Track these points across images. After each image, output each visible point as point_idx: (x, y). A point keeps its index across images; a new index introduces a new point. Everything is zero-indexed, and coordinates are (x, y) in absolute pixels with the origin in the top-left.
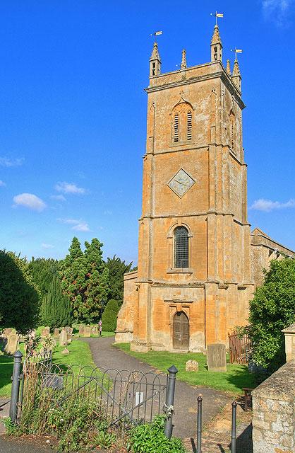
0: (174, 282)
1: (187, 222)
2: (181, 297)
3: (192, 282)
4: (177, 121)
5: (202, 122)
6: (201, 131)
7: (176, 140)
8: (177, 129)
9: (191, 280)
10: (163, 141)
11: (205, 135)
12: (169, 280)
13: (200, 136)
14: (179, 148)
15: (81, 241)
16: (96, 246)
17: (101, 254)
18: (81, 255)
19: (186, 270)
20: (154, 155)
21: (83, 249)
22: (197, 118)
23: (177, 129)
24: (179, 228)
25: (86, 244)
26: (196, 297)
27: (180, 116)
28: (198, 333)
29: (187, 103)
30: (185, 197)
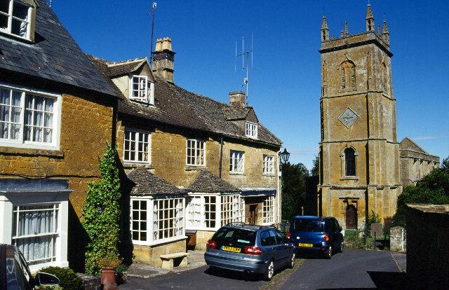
0: (346, 186)
1: (355, 145)
5: (362, 75)
6: (362, 81)
13: (361, 84)
22: (359, 72)
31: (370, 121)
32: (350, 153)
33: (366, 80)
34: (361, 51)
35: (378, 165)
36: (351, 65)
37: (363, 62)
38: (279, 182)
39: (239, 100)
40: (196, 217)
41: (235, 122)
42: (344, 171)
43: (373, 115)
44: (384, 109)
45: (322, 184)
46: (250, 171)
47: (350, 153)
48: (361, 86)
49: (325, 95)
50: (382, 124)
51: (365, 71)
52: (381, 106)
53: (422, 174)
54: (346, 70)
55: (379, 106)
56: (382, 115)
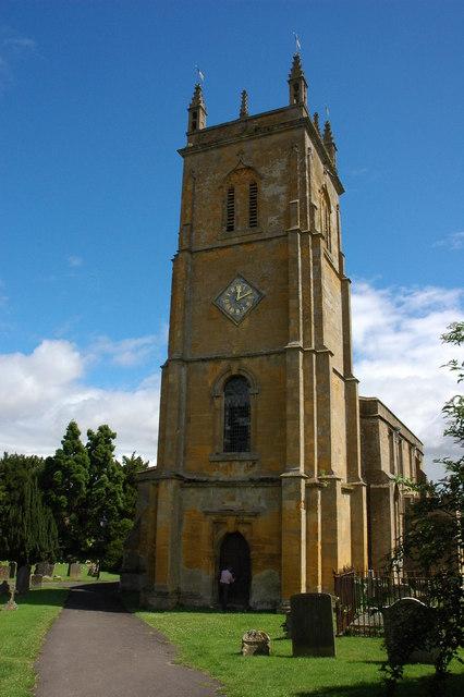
2: (235, 505)
3: (256, 477)
4: (231, 199)
5: (276, 198)
7: (230, 229)
8: (241, 244)
9: (254, 473)
11: (280, 218)
12: (214, 474)
13: (272, 219)
14: (236, 240)
15: (83, 428)
16: (104, 437)
17: (112, 450)
18: (78, 449)
19: (244, 455)
20: (191, 253)
21: (84, 440)
22: (267, 191)
23: (241, 244)
24: (234, 378)
25: (90, 433)
26: (263, 504)
27: (237, 190)
28: (264, 573)
29: (249, 168)
30: (245, 323)
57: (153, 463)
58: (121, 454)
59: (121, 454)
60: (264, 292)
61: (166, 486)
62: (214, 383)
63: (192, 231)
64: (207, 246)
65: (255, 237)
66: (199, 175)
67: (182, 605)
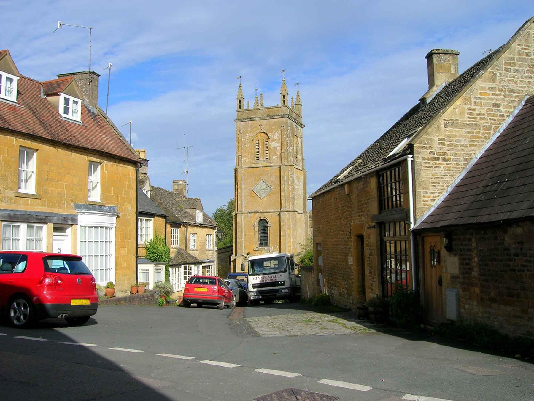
1: (267, 217)
5: (275, 148)
6: (276, 154)
10: (249, 159)
13: (274, 157)
14: (260, 165)
22: (274, 144)
31: (283, 194)
32: (263, 223)
33: (279, 154)
34: (275, 124)
35: (289, 236)
36: (264, 136)
37: (277, 136)
38: (215, 254)
39: (182, 187)
40: (274, 276)
41: (186, 210)
42: (258, 242)
43: (284, 187)
44: (296, 181)
45: (236, 255)
46: (200, 247)
47: (263, 223)
48: (275, 159)
49: (240, 166)
50: (294, 197)
51: (279, 144)
52: (293, 179)
53: (330, 195)
54: (260, 141)
55: (291, 179)
56: (293, 188)
57: (48, 260)
58: (88, 198)
59: (88, 198)
60: (272, 188)
61: (239, 259)
62: (254, 222)
63: (242, 158)
64: (249, 166)
65: (269, 165)
66: (243, 132)
67: (264, 399)
